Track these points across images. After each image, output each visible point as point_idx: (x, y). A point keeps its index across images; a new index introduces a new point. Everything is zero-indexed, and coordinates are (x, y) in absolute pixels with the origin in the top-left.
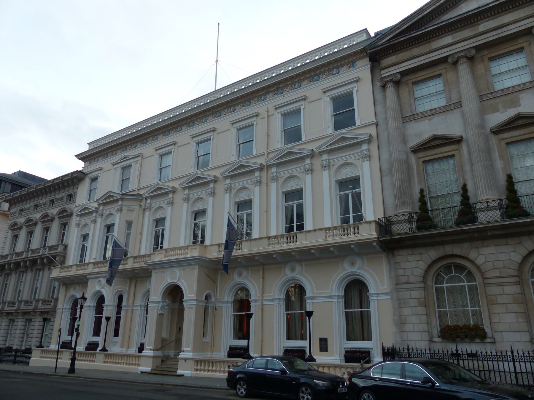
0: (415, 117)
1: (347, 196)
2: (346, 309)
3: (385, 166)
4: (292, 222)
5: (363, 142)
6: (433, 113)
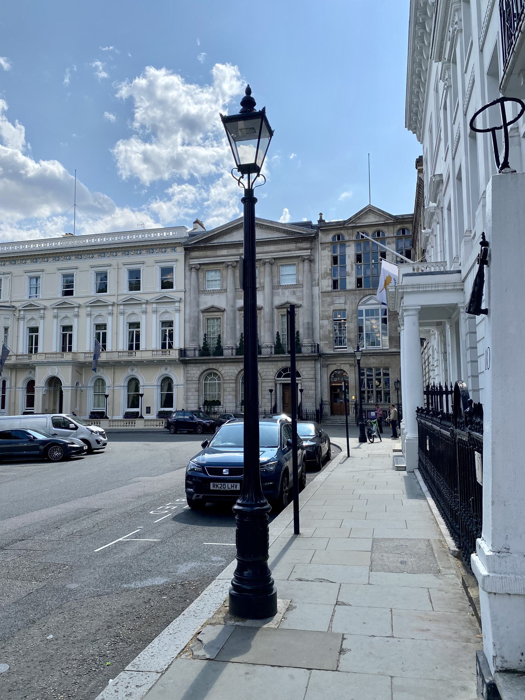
0: (205, 292)
1: (32, 336)
2: (161, 392)
3: (187, 317)
4: (32, 345)
5: (177, 301)
6: (213, 292)
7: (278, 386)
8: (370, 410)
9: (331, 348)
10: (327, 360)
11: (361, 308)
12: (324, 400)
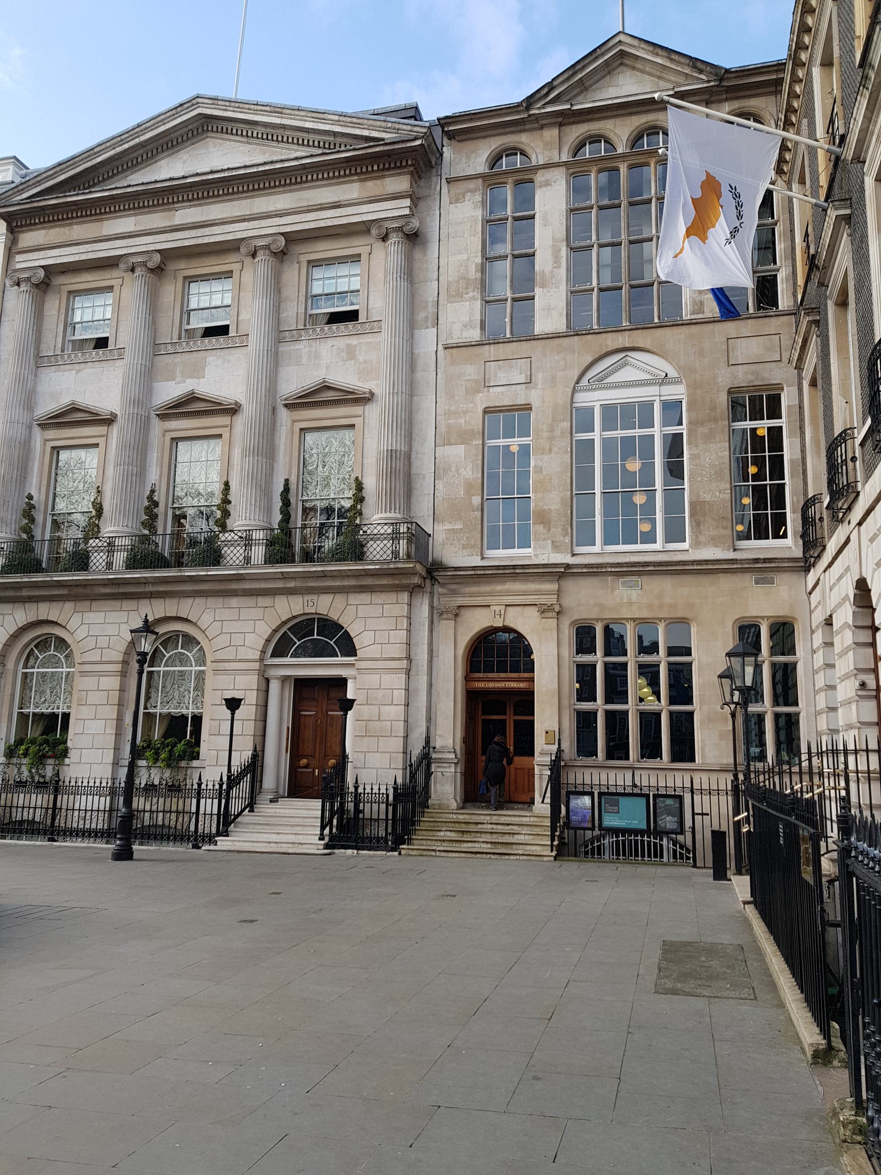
7: (275, 686)
8: (612, 790)
9: (472, 547)
10: (454, 593)
11: (584, 399)
12: (438, 743)
